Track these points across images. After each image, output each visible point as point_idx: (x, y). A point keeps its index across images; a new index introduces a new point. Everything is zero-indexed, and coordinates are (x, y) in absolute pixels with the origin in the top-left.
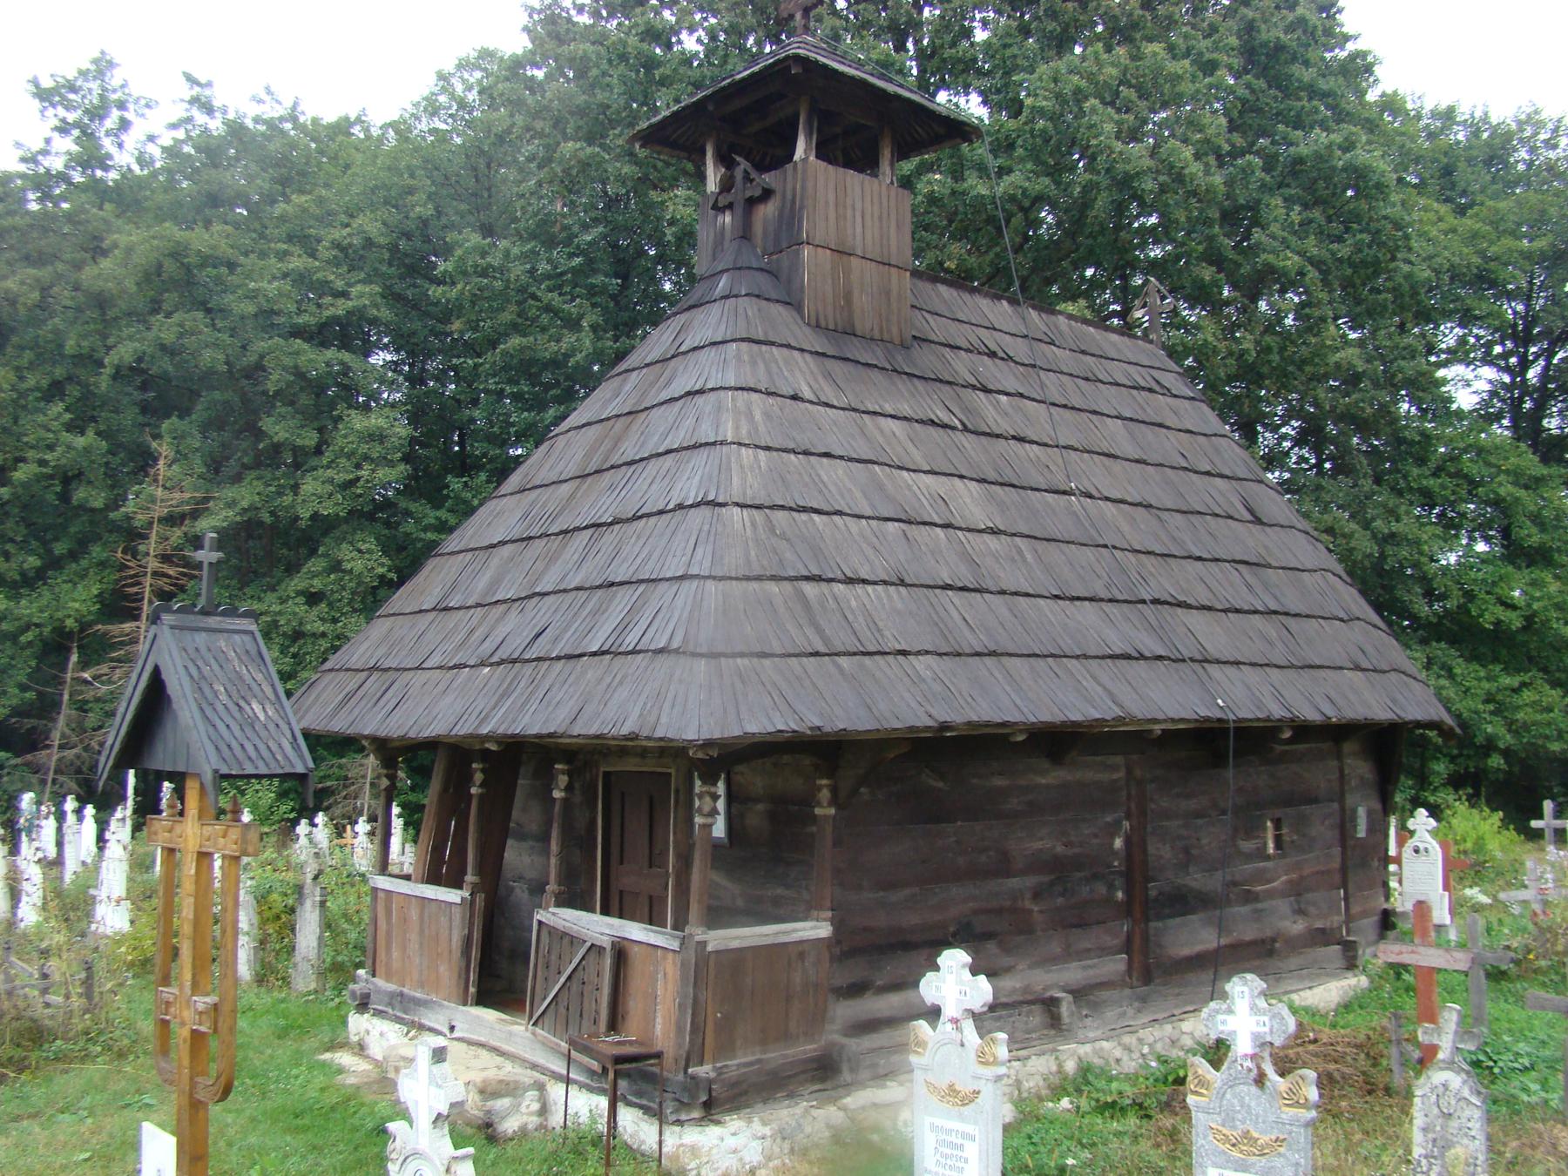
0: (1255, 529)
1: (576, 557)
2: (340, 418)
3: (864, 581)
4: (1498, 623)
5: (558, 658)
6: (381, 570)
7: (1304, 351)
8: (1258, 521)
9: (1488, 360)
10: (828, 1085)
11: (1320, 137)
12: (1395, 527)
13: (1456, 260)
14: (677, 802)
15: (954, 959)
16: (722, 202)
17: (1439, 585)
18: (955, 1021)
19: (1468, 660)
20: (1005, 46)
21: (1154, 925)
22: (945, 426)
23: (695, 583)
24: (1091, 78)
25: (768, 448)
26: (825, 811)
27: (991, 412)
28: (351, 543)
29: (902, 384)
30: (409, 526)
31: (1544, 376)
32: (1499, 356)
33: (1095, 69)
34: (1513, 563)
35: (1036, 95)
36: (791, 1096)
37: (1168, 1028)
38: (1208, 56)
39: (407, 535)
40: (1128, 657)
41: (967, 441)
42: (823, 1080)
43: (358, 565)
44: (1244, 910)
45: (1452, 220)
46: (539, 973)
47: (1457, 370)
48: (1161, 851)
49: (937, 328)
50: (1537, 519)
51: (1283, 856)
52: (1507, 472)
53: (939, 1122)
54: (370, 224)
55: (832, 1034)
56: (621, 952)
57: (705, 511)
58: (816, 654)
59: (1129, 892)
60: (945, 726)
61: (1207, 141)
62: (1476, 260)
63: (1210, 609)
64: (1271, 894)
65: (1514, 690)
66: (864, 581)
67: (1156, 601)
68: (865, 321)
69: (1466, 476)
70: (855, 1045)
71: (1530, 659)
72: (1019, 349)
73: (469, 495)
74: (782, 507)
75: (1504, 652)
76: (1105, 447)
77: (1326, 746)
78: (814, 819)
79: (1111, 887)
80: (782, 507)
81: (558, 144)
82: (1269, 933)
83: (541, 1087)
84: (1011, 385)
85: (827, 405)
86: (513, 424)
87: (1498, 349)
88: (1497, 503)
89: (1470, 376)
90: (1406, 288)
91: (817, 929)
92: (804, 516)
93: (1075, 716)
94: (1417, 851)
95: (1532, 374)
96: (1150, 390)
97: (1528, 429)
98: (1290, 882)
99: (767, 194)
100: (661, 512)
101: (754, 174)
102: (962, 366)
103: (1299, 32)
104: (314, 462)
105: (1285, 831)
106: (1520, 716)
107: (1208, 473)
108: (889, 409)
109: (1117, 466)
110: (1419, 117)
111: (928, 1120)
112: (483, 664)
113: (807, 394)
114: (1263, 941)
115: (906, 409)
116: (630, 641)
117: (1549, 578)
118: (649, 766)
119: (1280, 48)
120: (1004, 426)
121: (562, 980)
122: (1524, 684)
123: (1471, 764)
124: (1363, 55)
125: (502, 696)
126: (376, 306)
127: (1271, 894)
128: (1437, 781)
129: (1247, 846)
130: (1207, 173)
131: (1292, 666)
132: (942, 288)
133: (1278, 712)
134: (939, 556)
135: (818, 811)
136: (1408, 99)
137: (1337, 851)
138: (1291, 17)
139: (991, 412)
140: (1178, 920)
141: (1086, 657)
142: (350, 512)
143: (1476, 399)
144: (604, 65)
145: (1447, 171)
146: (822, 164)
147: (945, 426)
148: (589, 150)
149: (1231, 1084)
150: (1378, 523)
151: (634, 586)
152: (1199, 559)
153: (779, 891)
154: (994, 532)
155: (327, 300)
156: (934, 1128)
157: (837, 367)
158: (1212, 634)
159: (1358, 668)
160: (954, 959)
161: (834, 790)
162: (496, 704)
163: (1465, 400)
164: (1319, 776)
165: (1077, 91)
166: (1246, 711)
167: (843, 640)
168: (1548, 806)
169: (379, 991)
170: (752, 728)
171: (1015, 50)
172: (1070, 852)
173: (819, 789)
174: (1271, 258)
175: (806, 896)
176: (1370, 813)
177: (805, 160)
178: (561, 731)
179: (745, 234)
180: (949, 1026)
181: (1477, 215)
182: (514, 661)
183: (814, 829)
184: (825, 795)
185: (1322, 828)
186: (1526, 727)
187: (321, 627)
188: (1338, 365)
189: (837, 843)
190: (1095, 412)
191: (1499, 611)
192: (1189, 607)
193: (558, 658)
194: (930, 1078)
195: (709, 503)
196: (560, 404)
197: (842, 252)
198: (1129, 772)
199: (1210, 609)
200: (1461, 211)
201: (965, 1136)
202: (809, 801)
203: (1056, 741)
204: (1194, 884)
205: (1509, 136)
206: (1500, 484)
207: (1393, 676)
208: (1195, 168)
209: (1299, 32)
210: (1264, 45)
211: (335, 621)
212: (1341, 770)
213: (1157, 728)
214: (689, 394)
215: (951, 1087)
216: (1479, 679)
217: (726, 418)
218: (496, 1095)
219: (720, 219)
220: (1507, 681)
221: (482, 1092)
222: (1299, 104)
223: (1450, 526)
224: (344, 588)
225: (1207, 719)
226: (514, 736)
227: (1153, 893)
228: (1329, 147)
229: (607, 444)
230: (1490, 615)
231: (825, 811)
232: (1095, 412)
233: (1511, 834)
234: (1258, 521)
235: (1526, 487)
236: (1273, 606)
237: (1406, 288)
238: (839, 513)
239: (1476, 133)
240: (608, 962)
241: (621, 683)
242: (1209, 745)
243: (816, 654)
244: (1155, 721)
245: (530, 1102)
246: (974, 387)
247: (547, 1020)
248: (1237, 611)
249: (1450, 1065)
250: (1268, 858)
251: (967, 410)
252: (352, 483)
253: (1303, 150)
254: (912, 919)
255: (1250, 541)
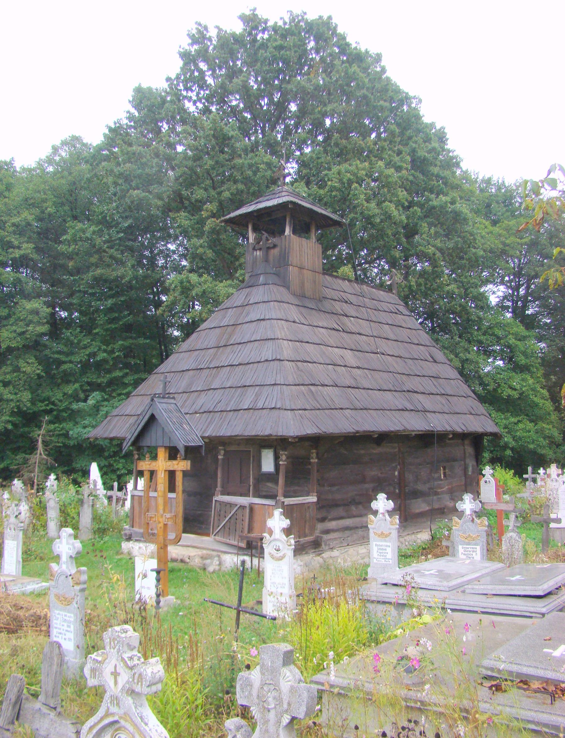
0: (434, 364)
1: (225, 376)
2: (16, 303)
3: (327, 385)
4: (509, 396)
5: (230, 411)
6: (38, 372)
7: (435, 285)
8: (435, 361)
9: (502, 283)
10: (317, 550)
11: (443, 198)
12: (469, 356)
13: (493, 246)
14: (253, 460)
15: (382, 496)
16: (257, 247)
17: (486, 380)
18: (383, 514)
19: (497, 411)
20: (318, 158)
21: (408, 502)
22: (337, 330)
23: (279, 387)
24: (355, 174)
25: (291, 341)
26: (314, 460)
27: (350, 324)
28: (24, 359)
29: (322, 315)
30: (47, 352)
31: (527, 294)
32: (508, 282)
33: (356, 171)
34: (515, 372)
35: (332, 181)
36: (306, 553)
37: (413, 536)
38: (399, 164)
39: (46, 355)
40: (403, 410)
41: (344, 335)
42: (315, 548)
43: (28, 369)
44: (435, 498)
45: (491, 228)
46: (216, 518)
47: (490, 286)
48: (409, 477)
49: (329, 293)
50: (524, 354)
51: (447, 479)
52: (513, 334)
53: (378, 543)
54: (27, 215)
55: (317, 533)
56: (252, 508)
57: (277, 362)
58: (319, 409)
59: (400, 490)
60: (358, 432)
61: (399, 201)
62: (501, 246)
63: (424, 393)
64: (443, 493)
65: (515, 424)
66: (327, 385)
67: (408, 391)
68: (308, 293)
69: (495, 335)
70: (325, 537)
71: (521, 410)
72: (353, 299)
73: (73, 338)
74: (299, 361)
75: (511, 408)
76: (385, 336)
77: (460, 441)
78: (310, 463)
79: (395, 488)
80: (299, 361)
81: (128, 191)
82: (442, 506)
83: (219, 556)
84: (354, 313)
85: (303, 324)
86: (92, 307)
87: (507, 278)
88: (509, 347)
89: (495, 290)
90: (474, 259)
91: (313, 499)
92: (305, 364)
93: (392, 429)
94: (486, 482)
95: (522, 292)
96: (396, 313)
97: (519, 313)
98: (449, 488)
99: (275, 246)
100: (259, 362)
101: (269, 238)
102: (338, 307)
103: (433, 153)
104: (5, 323)
105: (447, 471)
106: (518, 434)
107: (418, 344)
108: (321, 325)
109: (390, 343)
110: (476, 181)
111: (374, 543)
112: (196, 413)
113: (298, 321)
114: (441, 509)
115: (325, 325)
116: (260, 405)
117: (529, 378)
118: (242, 448)
119: (425, 159)
120: (354, 329)
121: (227, 519)
122: (519, 421)
123: (498, 454)
124: (456, 157)
125: (209, 423)
126: (32, 253)
127: (443, 493)
128: (485, 461)
129: (436, 476)
130: (400, 215)
131: (451, 413)
132: (327, 277)
133: (449, 429)
134: (344, 376)
135: (312, 460)
136: (472, 174)
137: (463, 478)
138: (430, 147)
139: (350, 324)
140: (415, 500)
141: (391, 410)
142: (24, 346)
143: (498, 300)
144: (149, 157)
145: (488, 206)
146: (295, 237)
147: (337, 330)
148: (144, 194)
149: (465, 522)
150: (461, 355)
151: (254, 388)
152: (419, 376)
153: (296, 488)
154: (358, 368)
155: (11, 250)
156: (376, 545)
157: (303, 310)
158: (427, 402)
159: (471, 414)
160: (382, 496)
161: (317, 454)
162: (207, 427)
163: (493, 300)
164: (457, 451)
165: (349, 180)
166: (439, 428)
167: (324, 405)
168: (530, 469)
169: (136, 533)
170: (309, 432)
171: (323, 160)
172: (383, 476)
173: (312, 453)
174: (423, 248)
175: (306, 489)
176: (473, 466)
177: (290, 235)
178: (240, 434)
179: (266, 260)
180: (381, 515)
181: (500, 227)
182: (210, 412)
183: (310, 467)
184: (314, 455)
185: (458, 471)
186: (520, 439)
187: (12, 397)
188: (448, 292)
189: (318, 471)
190: (380, 323)
191: (509, 391)
192: (418, 393)
193: (230, 411)
194: (375, 531)
195: (277, 360)
196: (113, 298)
197: (301, 268)
198: (399, 449)
199: (424, 393)
200: (494, 223)
201: (387, 546)
202: (308, 458)
203: (383, 438)
204: (419, 488)
205: (511, 191)
206: (510, 339)
207: (482, 417)
208: (395, 213)
209: (433, 153)
210: (419, 158)
211: (16, 394)
212: (464, 450)
213: (413, 433)
214: (258, 320)
215: (382, 532)
216: (502, 419)
217: (281, 330)
218: (206, 559)
219: (255, 253)
220: (513, 420)
221: (202, 558)
222: (433, 183)
223: (488, 353)
224: (20, 379)
225: (429, 431)
226: (220, 436)
227: (407, 491)
228: (446, 202)
229: (226, 336)
230: (506, 392)
231: (314, 460)
232: (380, 323)
233: (517, 479)
234: (435, 361)
235: (520, 340)
236: (443, 392)
237: (474, 259)
238: (315, 362)
239: (499, 189)
240: (248, 510)
241: (259, 419)
242: (427, 439)
243: (319, 409)
244: (414, 431)
245: (216, 561)
246: (343, 315)
247: (219, 533)
248: (432, 394)
249: (513, 531)
250: (441, 480)
251: (343, 324)
252: (24, 333)
253: (435, 203)
254: (338, 496)
255: (433, 369)
